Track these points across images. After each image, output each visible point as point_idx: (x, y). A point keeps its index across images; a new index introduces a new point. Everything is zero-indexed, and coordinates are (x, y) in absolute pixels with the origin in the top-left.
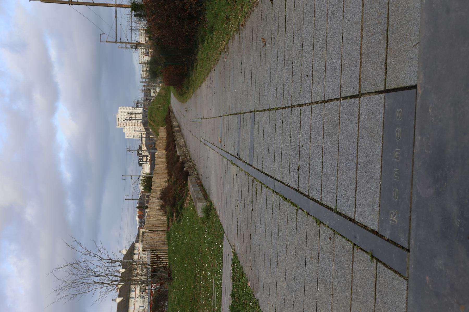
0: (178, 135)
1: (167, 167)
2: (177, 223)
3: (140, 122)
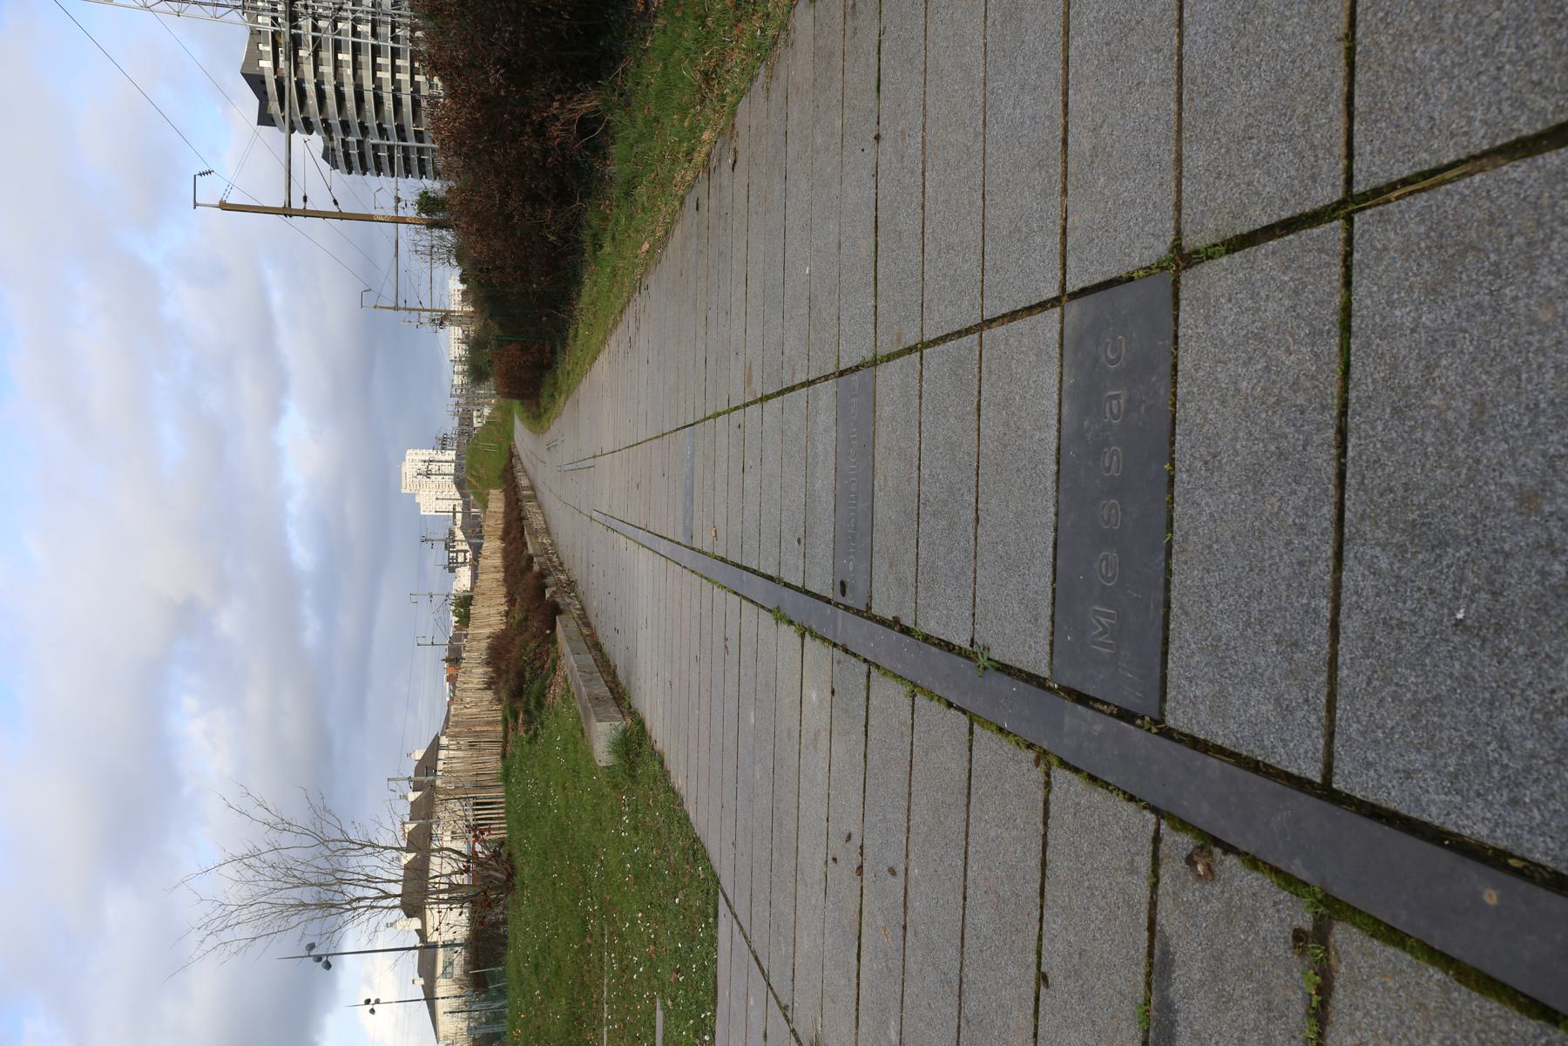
0: (530, 507)
1: (505, 580)
2: (529, 743)
3: (449, 480)
